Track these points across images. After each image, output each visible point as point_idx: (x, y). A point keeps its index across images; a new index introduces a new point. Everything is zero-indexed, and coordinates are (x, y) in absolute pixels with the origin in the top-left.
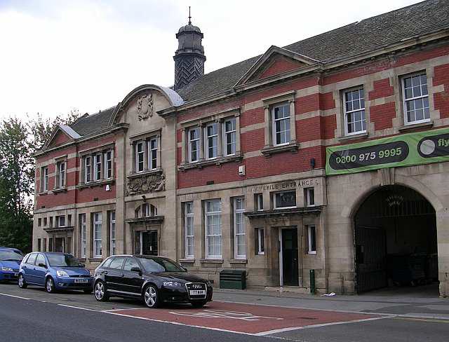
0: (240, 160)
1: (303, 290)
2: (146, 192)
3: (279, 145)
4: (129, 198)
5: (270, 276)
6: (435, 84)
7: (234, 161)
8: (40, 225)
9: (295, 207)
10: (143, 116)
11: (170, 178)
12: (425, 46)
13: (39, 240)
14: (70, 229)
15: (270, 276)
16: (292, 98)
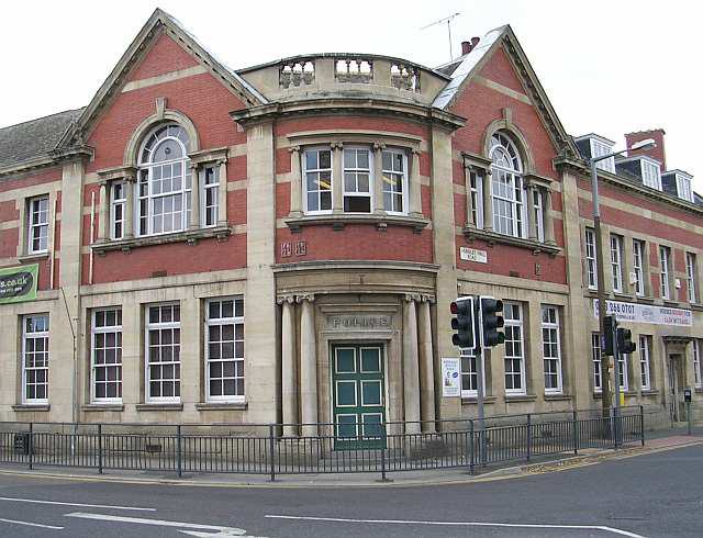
3: (37, 252)
7: (121, 250)
9: (522, 328)
11: (70, 268)
12: (516, 62)
16: (222, 157)
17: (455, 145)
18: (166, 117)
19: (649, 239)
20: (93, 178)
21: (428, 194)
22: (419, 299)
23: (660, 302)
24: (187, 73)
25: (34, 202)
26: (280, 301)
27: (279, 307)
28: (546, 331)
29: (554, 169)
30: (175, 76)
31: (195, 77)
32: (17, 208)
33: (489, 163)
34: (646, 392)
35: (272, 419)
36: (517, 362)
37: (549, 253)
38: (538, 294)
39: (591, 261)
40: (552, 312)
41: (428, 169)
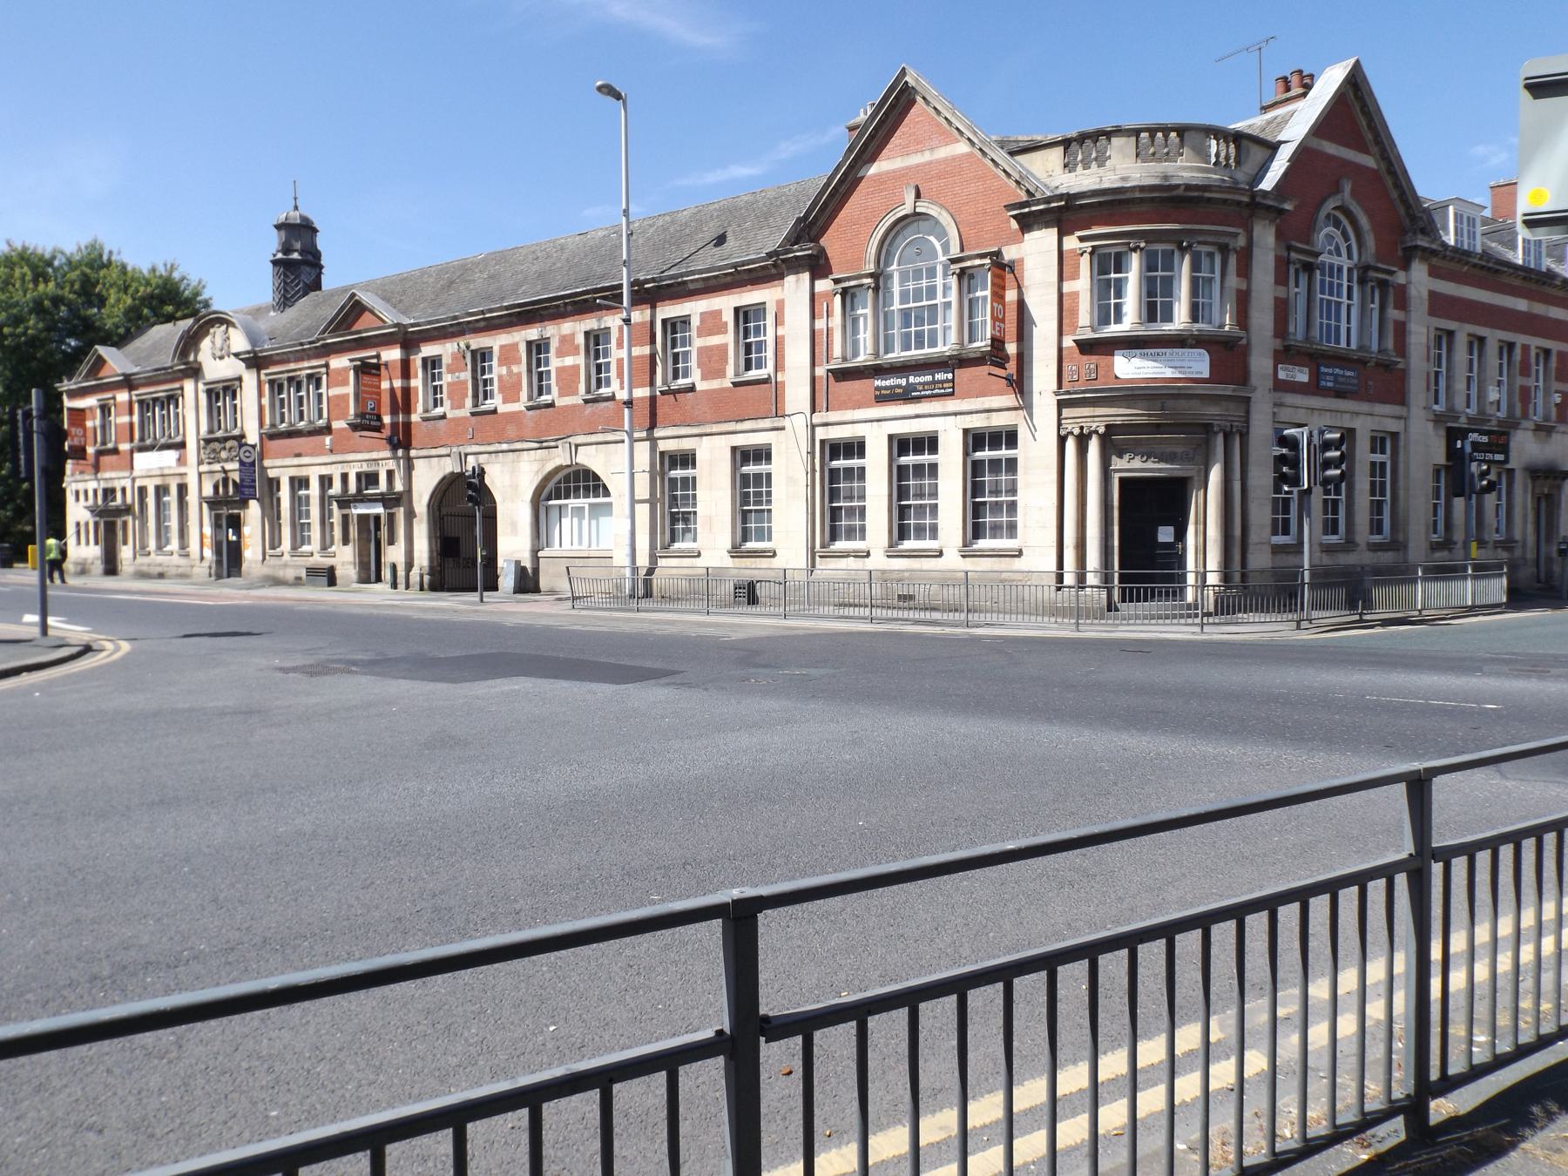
0: (328, 430)
1: (383, 587)
2: (226, 460)
4: (204, 468)
5: (166, 524)
6: (500, 364)
8: (77, 499)
10: (218, 354)
11: (797, 394)
13: (78, 524)
14: (128, 510)
15: (166, 524)
17: (1280, 235)
18: (917, 210)
19: (1520, 339)
20: (823, 285)
21: (1243, 302)
22: (1228, 429)
23: (1530, 425)
24: (943, 152)
25: (744, 315)
26: (1063, 433)
27: (1062, 441)
28: (1373, 464)
29: (1400, 253)
30: (926, 157)
31: (954, 158)
32: (724, 319)
33: (1317, 255)
34: (1500, 542)
35: (1053, 566)
36: (1335, 503)
37: (1387, 367)
38: (1367, 419)
39: (1437, 374)
40: (1383, 440)
41: (1245, 271)
